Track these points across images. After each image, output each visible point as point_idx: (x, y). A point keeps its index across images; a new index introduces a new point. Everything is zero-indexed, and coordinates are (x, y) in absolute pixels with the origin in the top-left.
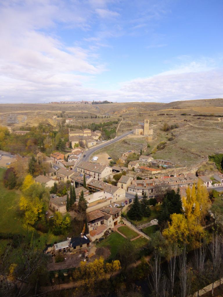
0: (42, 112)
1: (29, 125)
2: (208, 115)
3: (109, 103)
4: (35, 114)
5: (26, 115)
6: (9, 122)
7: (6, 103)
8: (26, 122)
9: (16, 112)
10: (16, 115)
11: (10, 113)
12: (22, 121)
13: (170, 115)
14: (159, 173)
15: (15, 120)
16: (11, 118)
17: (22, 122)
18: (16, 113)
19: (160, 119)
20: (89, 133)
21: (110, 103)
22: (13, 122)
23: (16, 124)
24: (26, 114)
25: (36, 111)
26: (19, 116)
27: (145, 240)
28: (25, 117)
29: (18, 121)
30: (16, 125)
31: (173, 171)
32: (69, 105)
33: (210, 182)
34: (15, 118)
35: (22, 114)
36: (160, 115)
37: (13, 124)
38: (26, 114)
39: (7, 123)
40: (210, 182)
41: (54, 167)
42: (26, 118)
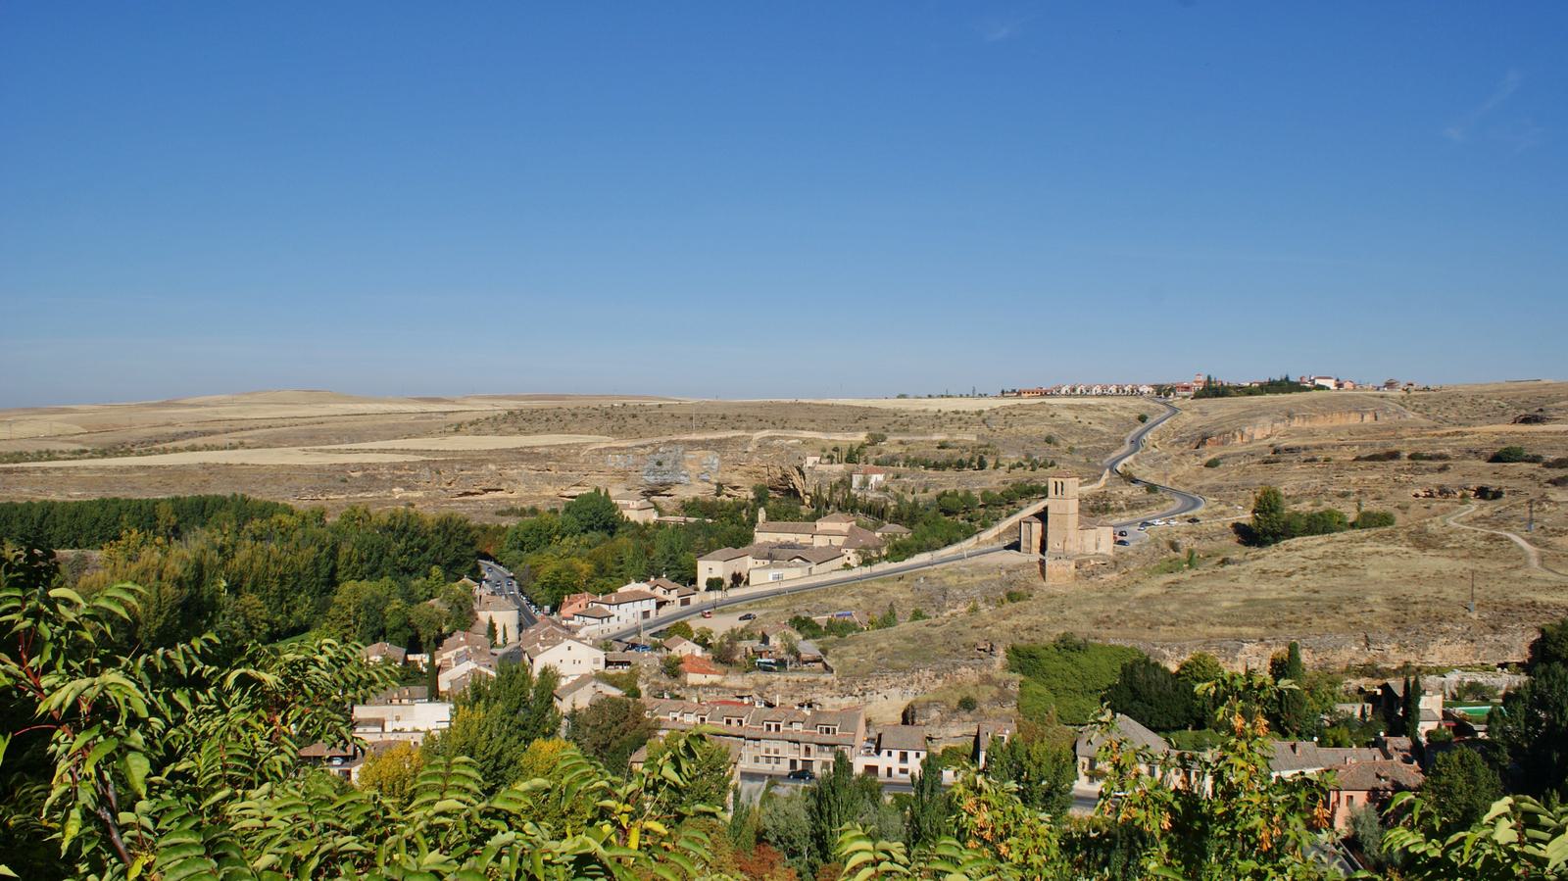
0: (782, 437)
6: (651, 479)
9: (686, 437)
10: (680, 450)
11: (664, 439)
13: (1430, 458)
14: (713, 685)
15: (675, 470)
16: (659, 464)
18: (684, 442)
22: (665, 477)
24: (719, 445)
25: (758, 435)
26: (689, 456)
28: (712, 458)
31: (769, 684)
33: (918, 755)
34: (675, 463)
35: (705, 445)
38: (719, 445)
39: (642, 482)
40: (918, 755)
42: (716, 461)
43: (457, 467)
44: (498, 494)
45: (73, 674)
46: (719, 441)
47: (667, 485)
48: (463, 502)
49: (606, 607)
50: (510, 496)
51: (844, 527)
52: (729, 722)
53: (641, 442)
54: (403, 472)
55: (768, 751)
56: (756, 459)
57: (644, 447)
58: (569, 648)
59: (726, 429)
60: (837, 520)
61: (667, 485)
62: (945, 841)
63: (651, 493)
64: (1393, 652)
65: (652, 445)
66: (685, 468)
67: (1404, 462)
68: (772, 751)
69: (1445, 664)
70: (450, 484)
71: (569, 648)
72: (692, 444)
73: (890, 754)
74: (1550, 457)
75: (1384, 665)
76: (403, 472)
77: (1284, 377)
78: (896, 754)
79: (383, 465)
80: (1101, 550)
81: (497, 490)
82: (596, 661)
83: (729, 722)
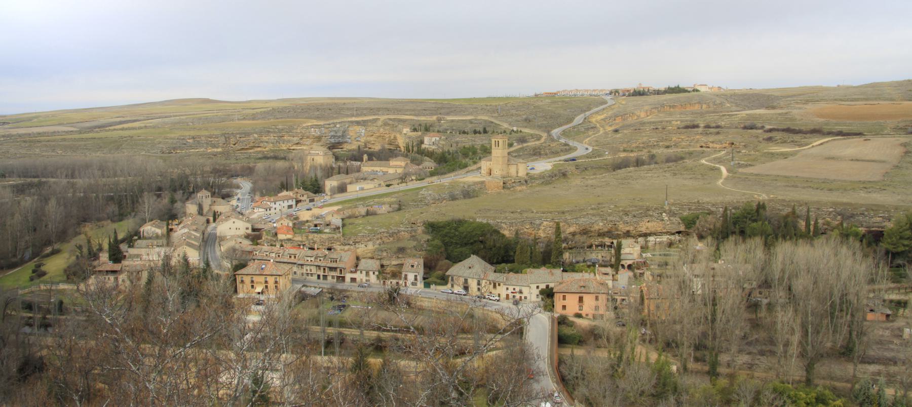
1: (370, 148)
2: (803, 128)
3: (684, 91)
4: (380, 123)
5: (364, 126)
6: (333, 140)
7: (798, 86)
8: (363, 140)
12: (358, 139)
17: (358, 141)
19: (674, 139)
20: (400, 167)
21: (689, 92)
22: (340, 139)
23: (346, 144)
27: (260, 372)
28: (362, 130)
29: (349, 138)
30: (347, 147)
32: (34, 115)
35: (358, 123)
36: (783, 130)
37: (341, 145)
39: (328, 142)
40: (374, 273)
41: (724, 299)
42: (363, 131)
43: (238, 136)
44: (259, 149)
45: (403, 341)
46: (364, 121)
47: (340, 143)
48: (241, 153)
49: (269, 203)
50: (264, 150)
51: (403, 164)
52: (290, 257)
53: (328, 123)
54: (212, 139)
55: (307, 270)
56: (382, 130)
57: (329, 124)
58: (234, 222)
59: (371, 115)
60: (401, 161)
61: (340, 143)
62: (461, 336)
63: (332, 147)
64: (621, 226)
65: (333, 123)
66: (349, 134)
67: (700, 130)
68: (309, 270)
69: (648, 232)
70: (235, 145)
71: (234, 222)
72: (352, 122)
73: (361, 272)
74: (768, 127)
75: (616, 233)
76: (212, 139)
77: (677, 86)
78: (364, 272)
79: (203, 136)
80: (520, 175)
81: (258, 147)
82: (247, 229)
83: (290, 257)
